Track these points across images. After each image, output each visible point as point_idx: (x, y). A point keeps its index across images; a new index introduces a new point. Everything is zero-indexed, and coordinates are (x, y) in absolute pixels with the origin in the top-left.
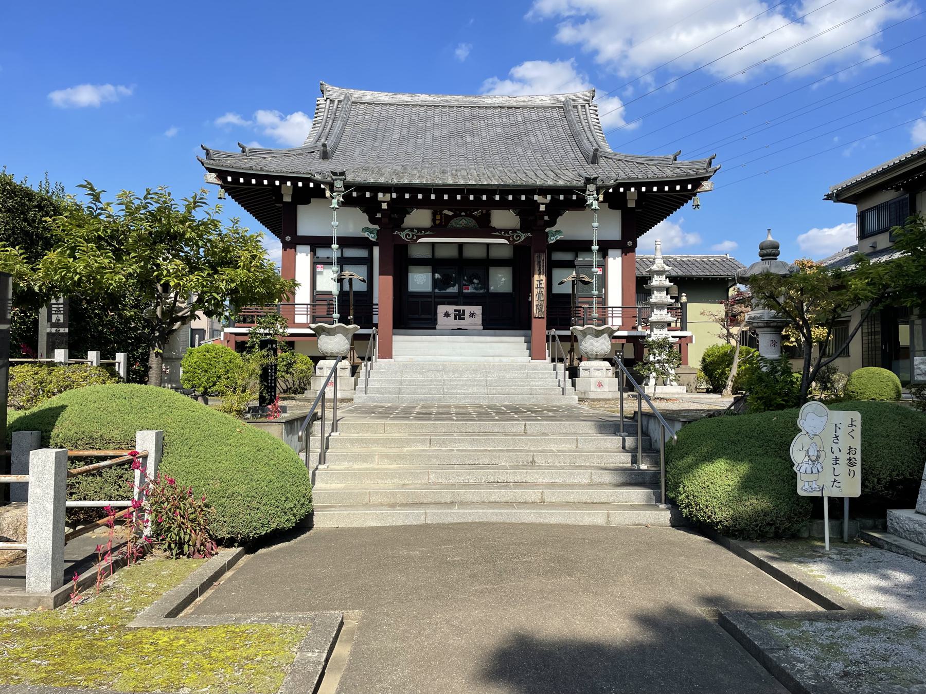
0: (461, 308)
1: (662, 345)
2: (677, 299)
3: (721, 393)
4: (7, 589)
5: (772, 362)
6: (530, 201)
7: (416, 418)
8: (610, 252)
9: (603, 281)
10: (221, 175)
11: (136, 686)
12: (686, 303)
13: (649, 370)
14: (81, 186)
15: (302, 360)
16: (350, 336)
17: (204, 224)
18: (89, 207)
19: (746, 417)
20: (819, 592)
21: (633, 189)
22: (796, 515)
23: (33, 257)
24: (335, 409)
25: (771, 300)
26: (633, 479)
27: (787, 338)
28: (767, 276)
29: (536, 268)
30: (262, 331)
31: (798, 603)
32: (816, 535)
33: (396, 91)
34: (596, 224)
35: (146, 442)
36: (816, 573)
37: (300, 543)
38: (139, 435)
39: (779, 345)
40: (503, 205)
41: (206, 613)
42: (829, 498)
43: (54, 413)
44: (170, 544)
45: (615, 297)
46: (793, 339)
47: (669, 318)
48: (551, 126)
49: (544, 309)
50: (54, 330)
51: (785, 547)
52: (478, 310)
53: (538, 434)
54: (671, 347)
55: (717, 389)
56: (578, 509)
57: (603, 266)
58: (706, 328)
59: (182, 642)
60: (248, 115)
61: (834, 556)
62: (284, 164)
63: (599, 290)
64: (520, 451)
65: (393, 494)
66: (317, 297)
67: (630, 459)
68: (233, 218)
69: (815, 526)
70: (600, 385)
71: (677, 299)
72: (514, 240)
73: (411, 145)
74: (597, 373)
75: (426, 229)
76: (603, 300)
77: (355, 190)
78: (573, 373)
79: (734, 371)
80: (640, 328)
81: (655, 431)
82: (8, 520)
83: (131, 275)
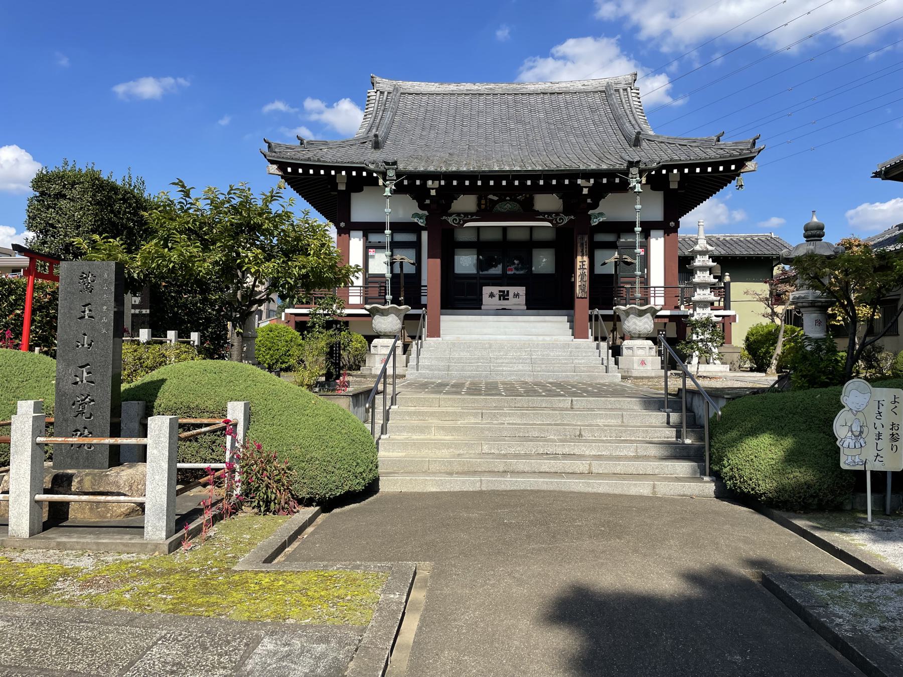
1: (706, 324)
2: (720, 278)
3: (765, 371)
4: (128, 537)
5: (817, 341)
6: (573, 184)
7: (467, 393)
8: (653, 233)
9: (645, 261)
10: (282, 166)
11: (249, 617)
12: (729, 283)
13: (692, 348)
14: (174, 184)
15: (357, 340)
16: (402, 316)
17: (279, 216)
18: (180, 202)
19: (790, 394)
20: (860, 558)
21: (675, 171)
22: (839, 487)
23: (131, 247)
24: (394, 384)
25: (816, 281)
26: (679, 453)
27: (834, 316)
28: (811, 257)
29: (579, 249)
30: (321, 311)
31: (842, 568)
32: (859, 508)
33: (442, 81)
34: (638, 207)
35: (236, 411)
36: (859, 543)
37: (368, 504)
38: (230, 405)
39: (824, 324)
40: (548, 189)
41: (296, 560)
42: (872, 472)
43: (158, 384)
44: (258, 503)
45: (657, 276)
46: (840, 318)
47: (712, 297)
48: (593, 110)
49: (587, 289)
50: (137, 311)
51: (828, 518)
52: (522, 290)
53: (584, 409)
54: (714, 326)
55: (761, 367)
56: (624, 479)
57: (646, 247)
58: (750, 307)
59: (281, 583)
60: (297, 102)
61: (876, 527)
62: (339, 155)
63: (642, 270)
64: (568, 425)
65: (450, 463)
66: (370, 280)
67: (674, 434)
68: (299, 210)
69: (858, 500)
70: (643, 363)
71: (720, 278)
73: (457, 133)
74: (640, 352)
75: (472, 214)
76: (646, 281)
77: (406, 179)
78: (616, 351)
79: (779, 350)
80: (682, 308)
81: (700, 407)
82: (125, 478)
83: (216, 263)
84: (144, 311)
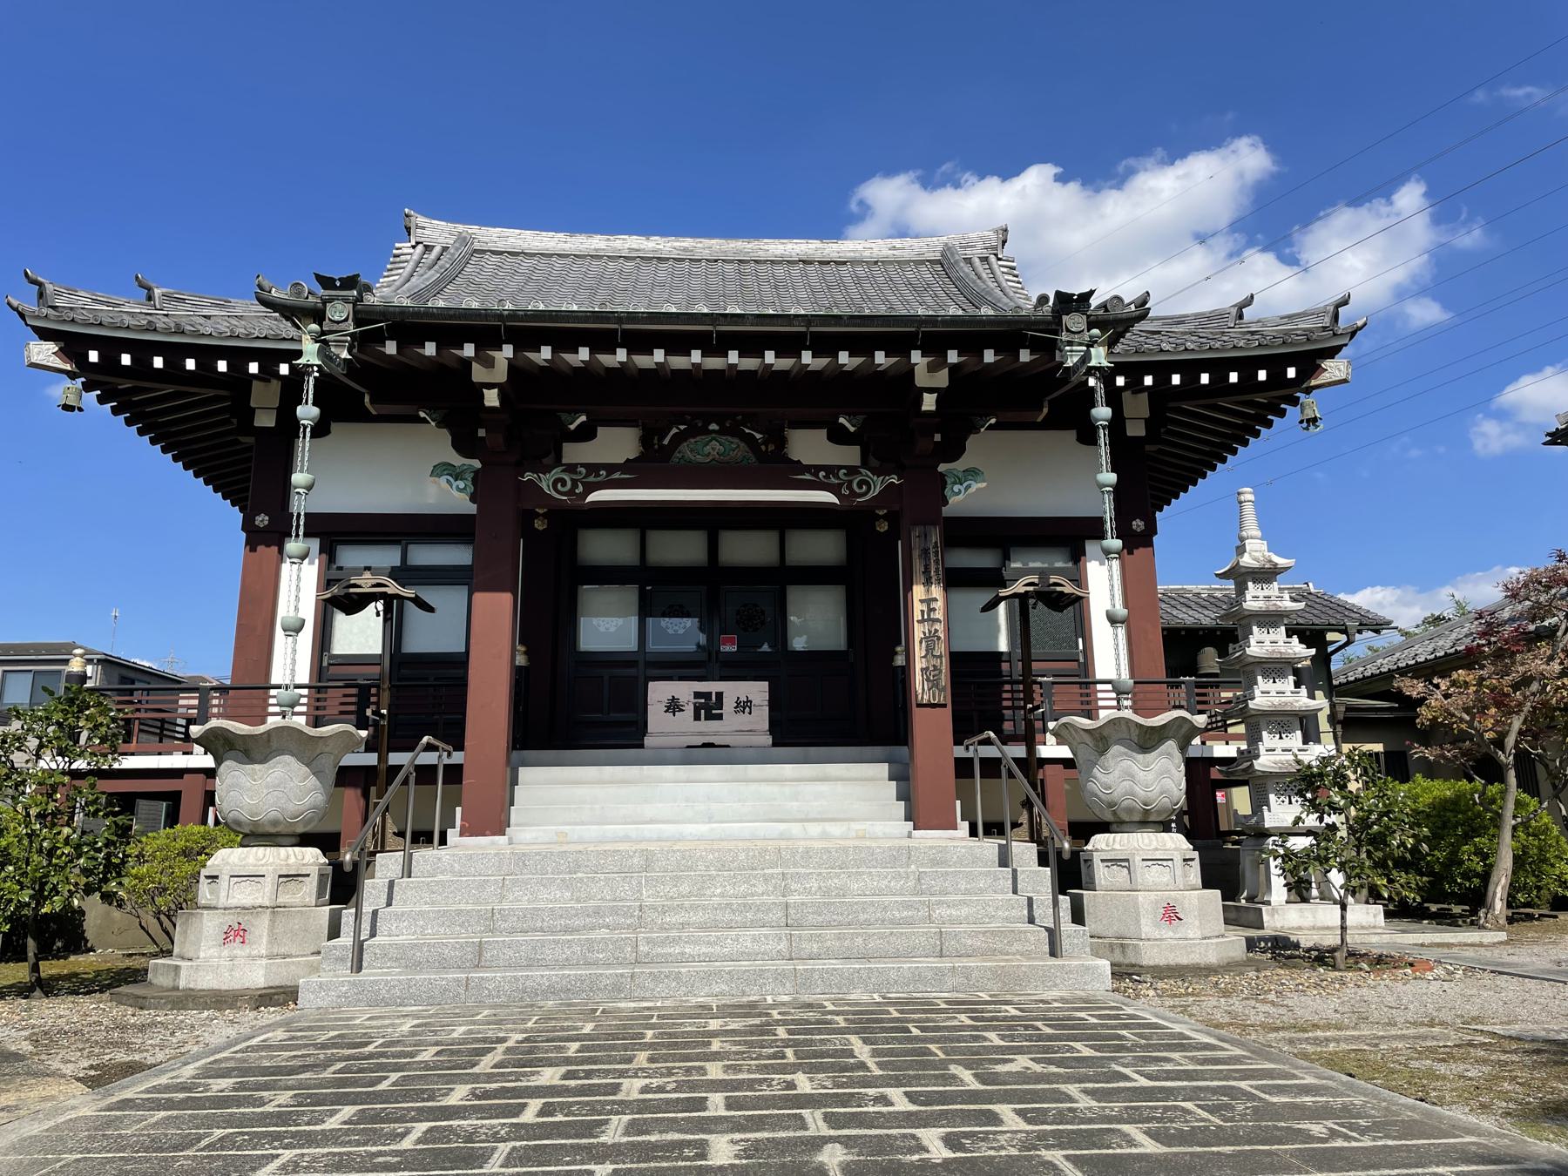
0: (712, 687)
10: (72, 345)
29: (918, 566)
33: (573, 228)
49: (945, 679)
52: (758, 692)
66: (328, 668)
70: (1171, 914)
72: (853, 494)
74: (1155, 875)
78: (1071, 875)
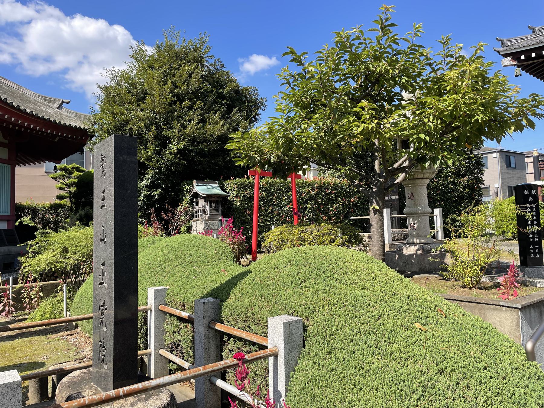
10: (515, 56)
84: (393, 197)
